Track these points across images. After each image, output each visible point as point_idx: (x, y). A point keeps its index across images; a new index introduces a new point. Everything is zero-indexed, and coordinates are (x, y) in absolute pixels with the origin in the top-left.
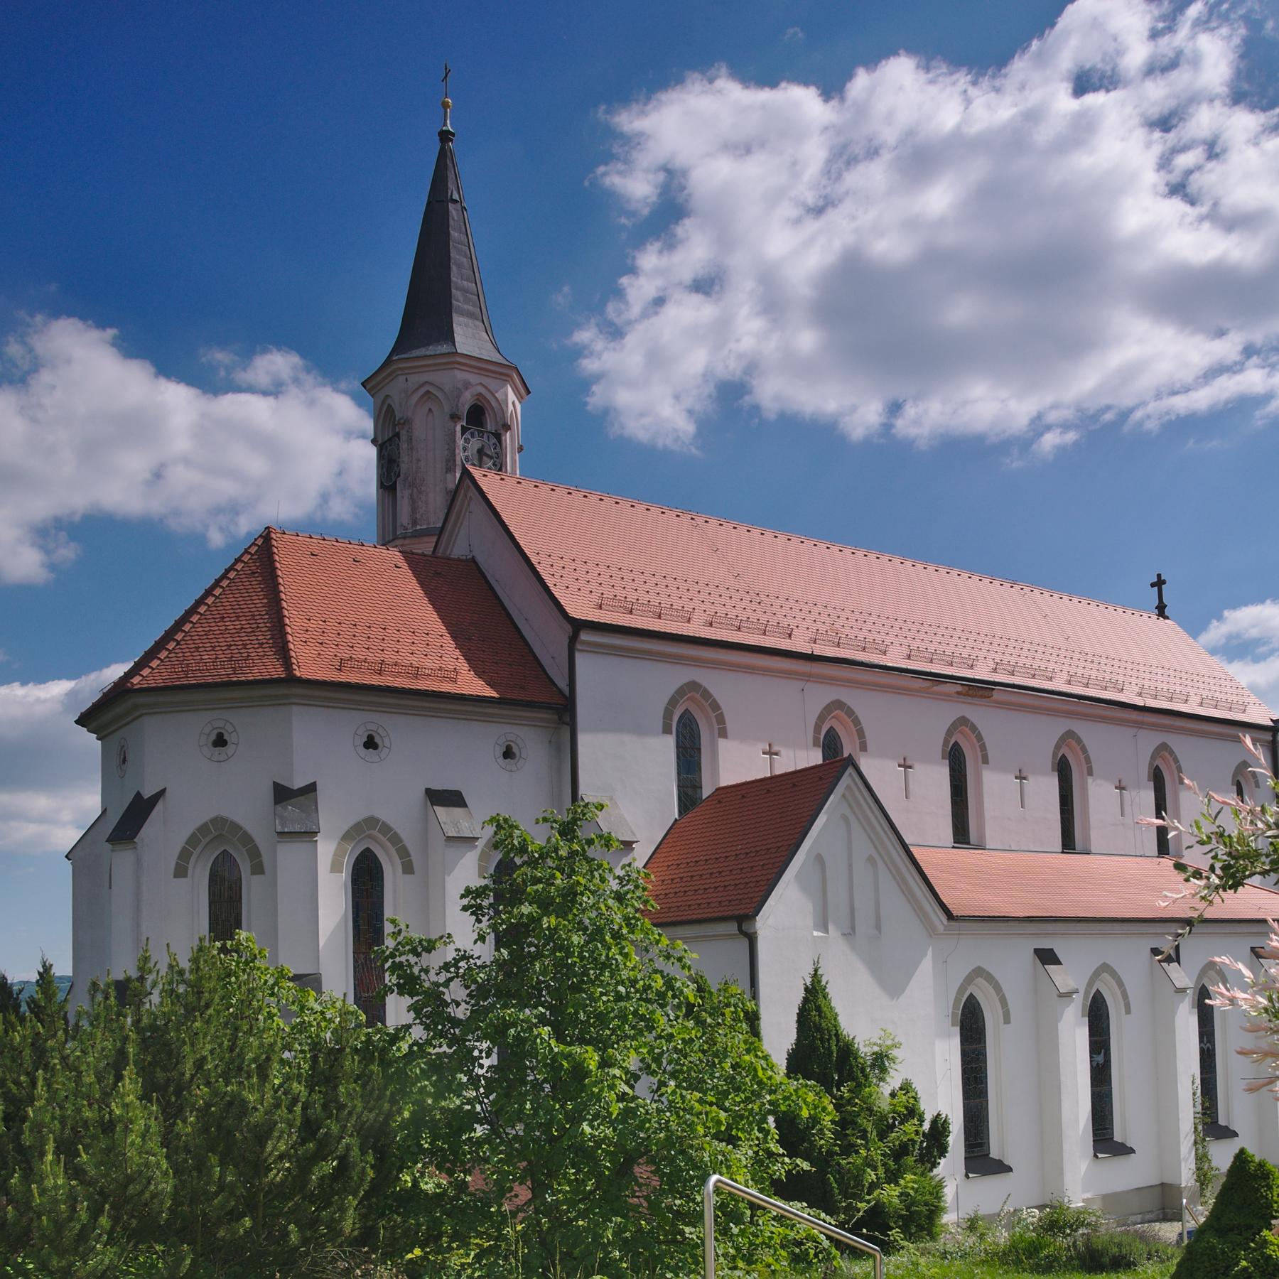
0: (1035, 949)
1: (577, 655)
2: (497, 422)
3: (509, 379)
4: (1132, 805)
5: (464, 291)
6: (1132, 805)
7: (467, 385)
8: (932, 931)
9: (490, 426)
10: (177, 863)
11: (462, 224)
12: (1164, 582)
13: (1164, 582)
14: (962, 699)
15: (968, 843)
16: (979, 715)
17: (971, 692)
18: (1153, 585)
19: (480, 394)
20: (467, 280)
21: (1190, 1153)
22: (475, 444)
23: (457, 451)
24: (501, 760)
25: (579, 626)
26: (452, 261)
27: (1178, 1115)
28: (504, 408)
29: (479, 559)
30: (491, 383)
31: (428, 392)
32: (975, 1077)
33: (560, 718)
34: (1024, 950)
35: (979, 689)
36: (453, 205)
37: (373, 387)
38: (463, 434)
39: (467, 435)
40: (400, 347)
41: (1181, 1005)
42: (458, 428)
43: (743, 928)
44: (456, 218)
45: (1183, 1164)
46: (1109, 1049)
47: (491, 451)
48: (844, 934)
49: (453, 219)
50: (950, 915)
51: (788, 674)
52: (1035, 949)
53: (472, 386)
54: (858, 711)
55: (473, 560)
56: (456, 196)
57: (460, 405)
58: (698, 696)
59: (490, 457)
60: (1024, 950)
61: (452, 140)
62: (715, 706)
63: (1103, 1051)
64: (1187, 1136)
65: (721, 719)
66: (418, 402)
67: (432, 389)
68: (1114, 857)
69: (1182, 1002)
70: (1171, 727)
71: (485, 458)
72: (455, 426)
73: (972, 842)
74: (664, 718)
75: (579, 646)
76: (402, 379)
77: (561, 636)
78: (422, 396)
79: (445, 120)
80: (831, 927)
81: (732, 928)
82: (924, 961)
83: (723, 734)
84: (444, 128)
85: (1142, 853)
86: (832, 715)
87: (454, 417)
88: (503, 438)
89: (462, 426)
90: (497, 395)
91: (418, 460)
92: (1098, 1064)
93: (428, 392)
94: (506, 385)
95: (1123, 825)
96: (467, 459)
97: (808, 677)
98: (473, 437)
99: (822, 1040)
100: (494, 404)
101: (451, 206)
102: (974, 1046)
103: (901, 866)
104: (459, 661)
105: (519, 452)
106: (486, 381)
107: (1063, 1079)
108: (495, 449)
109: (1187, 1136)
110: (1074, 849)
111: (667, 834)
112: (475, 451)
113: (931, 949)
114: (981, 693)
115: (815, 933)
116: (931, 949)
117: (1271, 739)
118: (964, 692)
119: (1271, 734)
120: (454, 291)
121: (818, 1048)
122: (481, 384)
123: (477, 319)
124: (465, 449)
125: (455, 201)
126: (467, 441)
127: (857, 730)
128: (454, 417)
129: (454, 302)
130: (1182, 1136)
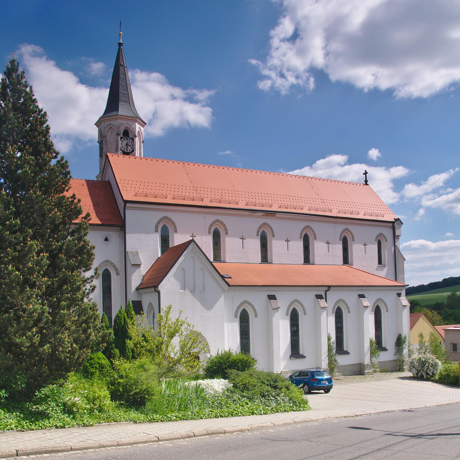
0: (268, 295)
1: (126, 210)
2: (132, 135)
3: (136, 121)
4: (332, 249)
5: (124, 94)
6: (332, 249)
7: (122, 124)
8: (223, 290)
9: (131, 136)
10: (116, 267)
11: (124, 73)
12: (367, 173)
13: (367, 173)
14: (264, 217)
15: (267, 262)
16: (270, 221)
17: (267, 215)
18: (364, 174)
19: (127, 127)
20: (125, 90)
21: (326, 358)
22: (125, 142)
23: (119, 145)
24: (104, 242)
25: (126, 202)
26: (120, 85)
27: (321, 346)
28: (135, 130)
29: (110, 181)
30: (130, 123)
31: (111, 127)
32: (245, 334)
33: (121, 229)
34: (264, 295)
35: (272, 214)
36: (122, 67)
37: (98, 124)
38: (121, 139)
39: (123, 140)
40: (104, 114)
41: (324, 312)
42: (119, 138)
43: (156, 289)
44: (122, 71)
45: (323, 362)
46: (299, 326)
47: (130, 144)
48: (191, 291)
49: (121, 71)
50: (229, 285)
51: (199, 212)
52: (268, 295)
53: (124, 124)
54: (225, 223)
55: (109, 181)
56: (122, 64)
57: (120, 130)
58: (167, 220)
59: (130, 146)
60: (264, 295)
61: (122, 46)
62: (173, 223)
63: (296, 326)
64: (325, 353)
65: (175, 227)
66: (108, 130)
67: (112, 126)
68: (323, 265)
69: (324, 311)
70: (350, 223)
71: (128, 146)
72: (118, 137)
73: (269, 261)
74: (155, 227)
75: (126, 208)
76: (103, 123)
77: (123, 204)
78: (109, 128)
79: (120, 39)
80: (186, 289)
81: (153, 289)
82: (221, 299)
83: (176, 231)
84: (120, 42)
85: (336, 264)
86: (216, 224)
87: (118, 134)
88: (134, 140)
89: (121, 137)
90: (132, 126)
91: (109, 148)
92: (294, 330)
93: (111, 127)
94: (135, 123)
95: (328, 255)
96: (122, 147)
97: (206, 213)
98: (124, 139)
99: (119, 320)
100: (131, 129)
101: (121, 67)
102: (245, 324)
103: (212, 271)
104: (93, 213)
105: (143, 143)
106: (128, 122)
107: (274, 334)
108: (132, 143)
109: (325, 353)
110: (310, 263)
111: (155, 262)
112: (125, 144)
113: (223, 295)
114: (271, 215)
115: (181, 291)
116: (223, 295)
117: (392, 225)
118: (265, 215)
119: (392, 224)
120: (120, 94)
121: (117, 322)
122: (127, 123)
123: (128, 103)
124: (121, 144)
125: (122, 65)
126: (122, 141)
127: (224, 229)
128: (118, 134)
129: (120, 98)
130: (323, 354)
